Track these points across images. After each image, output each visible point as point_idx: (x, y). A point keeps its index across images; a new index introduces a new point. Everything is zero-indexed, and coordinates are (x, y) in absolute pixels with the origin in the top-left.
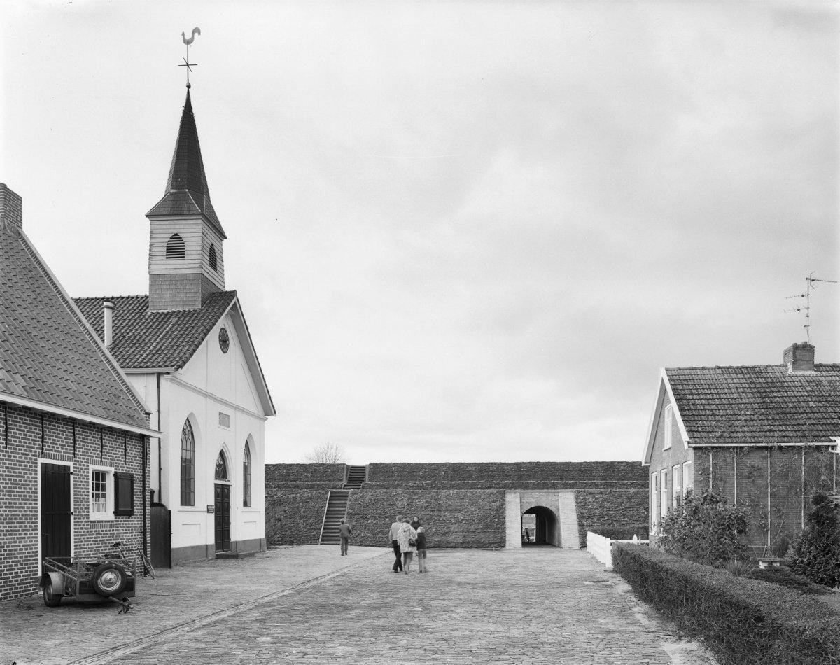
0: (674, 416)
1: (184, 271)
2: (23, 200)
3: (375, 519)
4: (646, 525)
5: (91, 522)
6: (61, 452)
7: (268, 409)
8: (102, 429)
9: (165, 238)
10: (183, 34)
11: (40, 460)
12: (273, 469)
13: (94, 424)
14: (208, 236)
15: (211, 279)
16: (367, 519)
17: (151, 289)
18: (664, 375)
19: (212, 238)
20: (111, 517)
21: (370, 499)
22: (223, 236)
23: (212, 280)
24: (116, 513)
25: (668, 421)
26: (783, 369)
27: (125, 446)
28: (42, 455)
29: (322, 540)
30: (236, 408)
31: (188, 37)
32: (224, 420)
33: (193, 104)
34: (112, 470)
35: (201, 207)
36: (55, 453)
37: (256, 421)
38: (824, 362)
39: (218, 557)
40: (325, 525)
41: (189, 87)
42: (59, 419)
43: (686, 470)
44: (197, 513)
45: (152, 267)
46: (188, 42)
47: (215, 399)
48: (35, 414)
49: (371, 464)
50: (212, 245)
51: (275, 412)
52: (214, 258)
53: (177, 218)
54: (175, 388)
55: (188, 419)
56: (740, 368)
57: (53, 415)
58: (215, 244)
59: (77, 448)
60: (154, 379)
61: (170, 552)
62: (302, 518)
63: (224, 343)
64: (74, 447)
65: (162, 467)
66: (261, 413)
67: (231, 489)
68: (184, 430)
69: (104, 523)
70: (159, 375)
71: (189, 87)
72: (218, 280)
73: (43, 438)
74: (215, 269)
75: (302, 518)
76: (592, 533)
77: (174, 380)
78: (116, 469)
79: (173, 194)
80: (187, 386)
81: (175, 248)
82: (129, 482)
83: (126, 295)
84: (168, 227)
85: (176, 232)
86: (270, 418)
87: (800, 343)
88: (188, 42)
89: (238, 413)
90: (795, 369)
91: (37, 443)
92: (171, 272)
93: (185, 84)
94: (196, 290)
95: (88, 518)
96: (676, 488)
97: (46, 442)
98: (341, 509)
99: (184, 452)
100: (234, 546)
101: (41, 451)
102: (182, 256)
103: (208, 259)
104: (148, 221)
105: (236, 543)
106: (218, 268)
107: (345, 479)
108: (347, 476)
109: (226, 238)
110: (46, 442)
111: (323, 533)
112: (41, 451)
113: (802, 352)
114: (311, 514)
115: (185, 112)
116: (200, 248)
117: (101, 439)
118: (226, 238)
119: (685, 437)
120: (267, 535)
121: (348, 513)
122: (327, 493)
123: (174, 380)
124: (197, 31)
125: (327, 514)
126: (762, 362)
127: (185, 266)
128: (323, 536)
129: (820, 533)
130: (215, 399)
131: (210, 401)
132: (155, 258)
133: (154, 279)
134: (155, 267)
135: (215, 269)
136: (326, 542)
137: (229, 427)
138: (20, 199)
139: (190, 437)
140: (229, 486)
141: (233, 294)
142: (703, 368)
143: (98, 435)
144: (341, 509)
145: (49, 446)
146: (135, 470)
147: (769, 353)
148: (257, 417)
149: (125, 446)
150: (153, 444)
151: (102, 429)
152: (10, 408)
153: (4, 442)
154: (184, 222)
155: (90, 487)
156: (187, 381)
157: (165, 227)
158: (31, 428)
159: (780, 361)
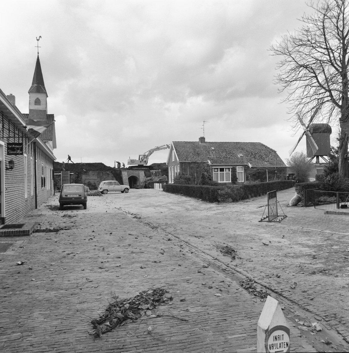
0: (175, 154)
9: (34, 99)
10: (37, 38)
17: (29, 112)
18: (172, 142)
25: (173, 154)
26: (199, 143)
31: (38, 39)
38: (207, 141)
41: (38, 53)
43: (178, 168)
46: (38, 40)
56: (190, 142)
61: (348, 176)
71: (38, 53)
79: (36, 86)
81: (37, 102)
86: (55, 149)
87: (202, 137)
88: (38, 40)
90: (201, 143)
96: (176, 171)
102: (40, 105)
113: (202, 139)
119: (178, 160)
124: (40, 37)
126: (194, 141)
129: (203, 181)
133: (30, 110)
134: (31, 107)
142: (181, 142)
147: (196, 139)
159: (198, 141)
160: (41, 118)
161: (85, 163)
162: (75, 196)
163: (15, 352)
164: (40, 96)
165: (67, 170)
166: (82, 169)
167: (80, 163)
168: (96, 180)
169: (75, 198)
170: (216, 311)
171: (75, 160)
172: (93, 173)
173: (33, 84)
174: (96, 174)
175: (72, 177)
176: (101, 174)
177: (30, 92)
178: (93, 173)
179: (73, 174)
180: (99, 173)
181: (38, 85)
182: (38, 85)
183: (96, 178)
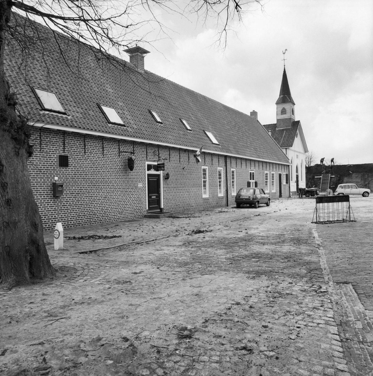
1: (286, 118)
4: (65, 244)
8: (119, 141)
9: (280, 109)
11: (147, 163)
22: (294, 104)
24: (286, 183)
27: (147, 150)
28: (147, 160)
30: (299, 152)
31: (284, 52)
32: (297, 156)
33: (286, 70)
35: (291, 100)
46: (284, 53)
48: (145, 144)
57: (152, 144)
59: (87, 149)
64: (85, 149)
70: (286, 149)
73: (64, 144)
81: (283, 112)
83: (268, 124)
91: (61, 147)
93: (284, 65)
97: (66, 147)
102: (285, 113)
110: (66, 147)
115: (284, 73)
117: (103, 144)
133: (278, 120)
141: (298, 122)
143: (101, 142)
145: (106, 153)
146: (288, 173)
149: (147, 150)
150: (290, 166)
151: (133, 143)
152: (136, 143)
153: (40, 147)
155: (202, 174)
158: (110, 146)
160: (287, 126)
161: (353, 165)
162: (246, 197)
163: (330, 371)
164: (287, 106)
165: (327, 173)
166: (349, 170)
167: (348, 165)
168: (359, 182)
169: (246, 199)
170: (118, 242)
171: (338, 162)
172: (357, 176)
173: (280, 96)
174: (360, 176)
175: (333, 179)
176: (366, 176)
177: (277, 103)
178: (357, 176)
179: (334, 177)
180: (363, 175)
181: (285, 95)
182: (285, 95)
183: (360, 181)
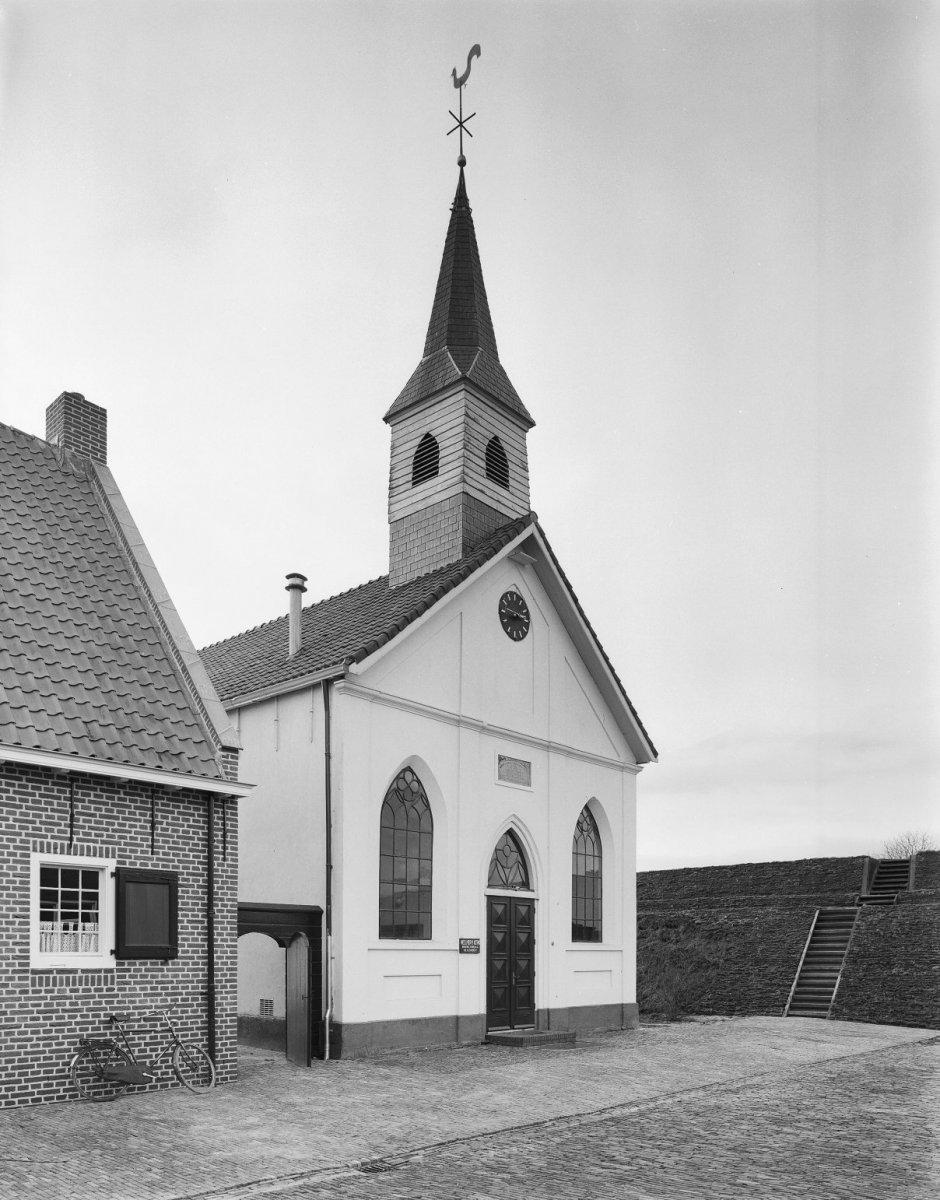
2: (108, 414)
3: (908, 966)
5: (34, 972)
6: (46, 837)
7: (641, 750)
9: (410, 448)
12: (730, 873)
13: (190, 790)
14: (481, 421)
15: (488, 502)
16: (890, 965)
19: (497, 425)
20: (110, 962)
21: (901, 924)
23: (495, 505)
24: (119, 952)
29: (791, 1008)
34: (111, 864)
36: (52, 841)
37: (616, 775)
39: (489, 1041)
40: (801, 978)
41: (462, 163)
42: (112, 785)
44: (608, 953)
45: (395, 507)
47: (484, 729)
49: (921, 854)
50: (496, 438)
51: (655, 754)
52: (498, 464)
53: (427, 405)
54: (362, 705)
55: (586, 807)
58: (501, 435)
60: (319, 695)
62: (757, 962)
63: (514, 618)
65: (333, 863)
66: (624, 756)
67: (538, 906)
68: (578, 823)
69: (80, 974)
71: (462, 163)
72: (510, 504)
74: (504, 484)
75: (757, 962)
76: (640, 852)
77: (349, 689)
78: (119, 862)
80: (394, 702)
82: (165, 889)
84: (417, 426)
85: (425, 431)
89: (557, 760)
92: (420, 506)
94: (455, 527)
95: (28, 964)
98: (838, 945)
99: (581, 859)
100: (542, 1019)
101: (222, 856)
103: (483, 464)
104: (388, 428)
105: (548, 1011)
106: (511, 482)
107: (864, 888)
108: (869, 879)
109: (532, 424)
111: (796, 993)
112: (66, 843)
114: (774, 956)
116: (460, 446)
118: (532, 424)
120: (641, 997)
121: (851, 952)
122: (812, 912)
123: (349, 689)
125: (807, 955)
127: (439, 488)
128: (794, 1000)
130: (484, 729)
131: (467, 734)
132: (397, 491)
135: (504, 484)
136: (798, 1013)
137: (529, 784)
138: (102, 413)
139: (592, 835)
140: (532, 900)
144: (838, 945)
148: (622, 768)
154: (437, 407)
156: (397, 693)
157: (411, 429)
